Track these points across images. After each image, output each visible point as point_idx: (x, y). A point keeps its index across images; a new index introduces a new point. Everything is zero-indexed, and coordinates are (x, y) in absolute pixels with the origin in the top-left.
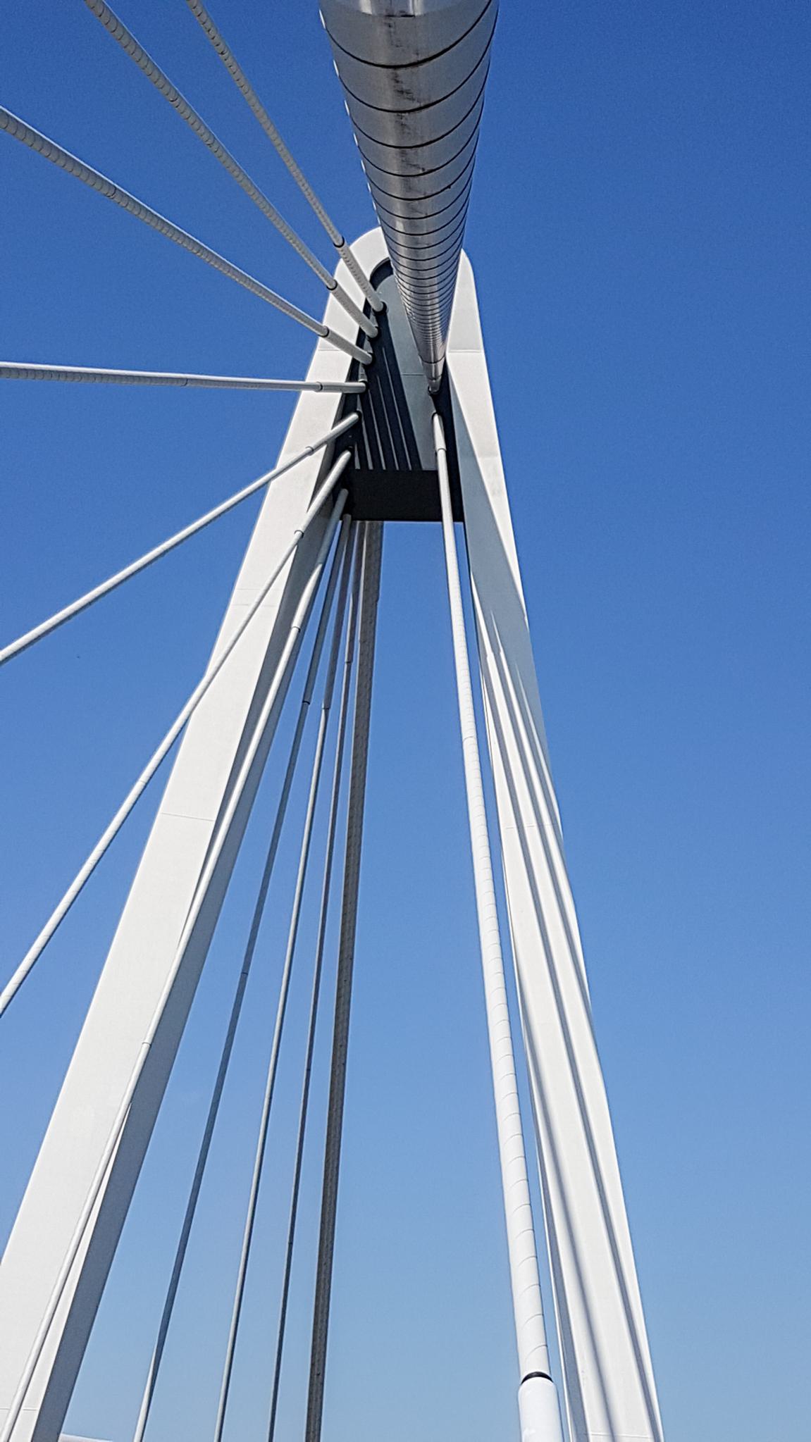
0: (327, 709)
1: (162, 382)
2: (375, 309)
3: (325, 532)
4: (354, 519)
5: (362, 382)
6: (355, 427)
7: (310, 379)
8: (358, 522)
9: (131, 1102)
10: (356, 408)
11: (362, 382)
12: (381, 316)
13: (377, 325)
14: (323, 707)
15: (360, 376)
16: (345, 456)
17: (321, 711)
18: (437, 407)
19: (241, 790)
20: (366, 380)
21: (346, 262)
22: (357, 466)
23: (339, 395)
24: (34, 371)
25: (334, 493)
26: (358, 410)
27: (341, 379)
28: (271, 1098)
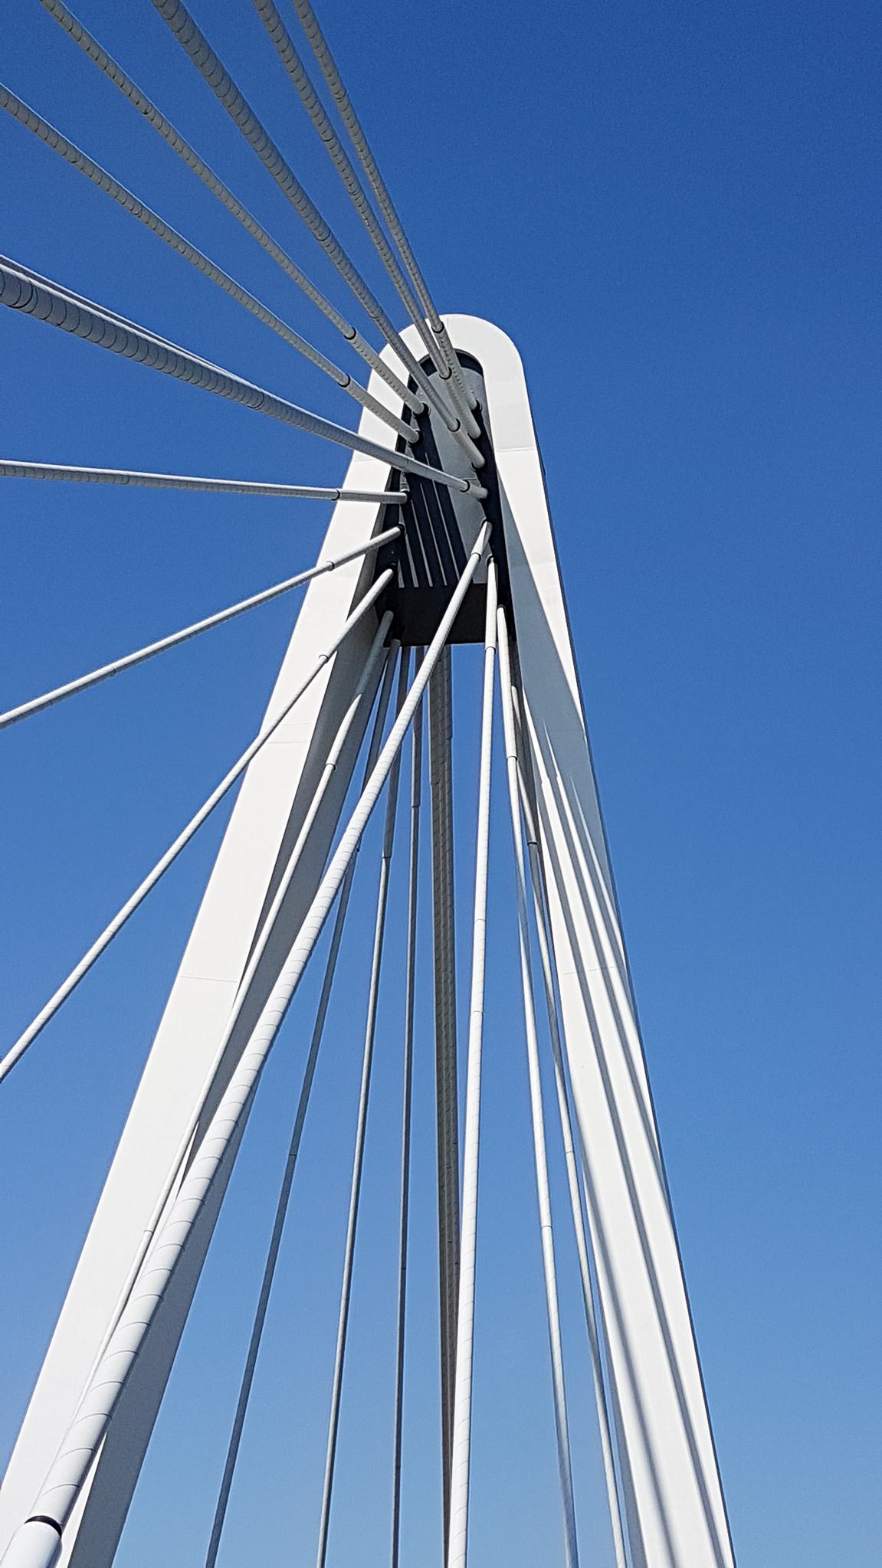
0: (387, 858)
1: (174, 485)
2: (416, 412)
3: (372, 642)
4: (406, 646)
5: (404, 492)
6: (397, 540)
7: (348, 486)
8: (413, 648)
9: (198, 1121)
10: (398, 521)
11: (404, 492)
12: (423, 418)
13: (418, 429)
14: (383, 856)
15: (401, 486)
16: (388, 573)
17: (382, 861)
18: (486, 515)
19: (277, 910)
20: (408, 490)
21: (379, 372)
22: (401, 585)
23: (378, 505)
24: (199, 482)
25: (378, 604)
26: (400, 523)
27: (379, 487)
28: (347, 1299)
